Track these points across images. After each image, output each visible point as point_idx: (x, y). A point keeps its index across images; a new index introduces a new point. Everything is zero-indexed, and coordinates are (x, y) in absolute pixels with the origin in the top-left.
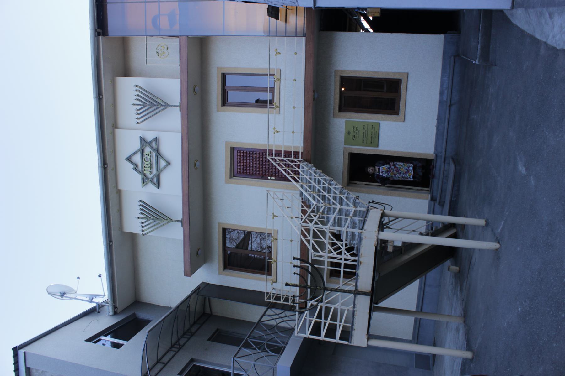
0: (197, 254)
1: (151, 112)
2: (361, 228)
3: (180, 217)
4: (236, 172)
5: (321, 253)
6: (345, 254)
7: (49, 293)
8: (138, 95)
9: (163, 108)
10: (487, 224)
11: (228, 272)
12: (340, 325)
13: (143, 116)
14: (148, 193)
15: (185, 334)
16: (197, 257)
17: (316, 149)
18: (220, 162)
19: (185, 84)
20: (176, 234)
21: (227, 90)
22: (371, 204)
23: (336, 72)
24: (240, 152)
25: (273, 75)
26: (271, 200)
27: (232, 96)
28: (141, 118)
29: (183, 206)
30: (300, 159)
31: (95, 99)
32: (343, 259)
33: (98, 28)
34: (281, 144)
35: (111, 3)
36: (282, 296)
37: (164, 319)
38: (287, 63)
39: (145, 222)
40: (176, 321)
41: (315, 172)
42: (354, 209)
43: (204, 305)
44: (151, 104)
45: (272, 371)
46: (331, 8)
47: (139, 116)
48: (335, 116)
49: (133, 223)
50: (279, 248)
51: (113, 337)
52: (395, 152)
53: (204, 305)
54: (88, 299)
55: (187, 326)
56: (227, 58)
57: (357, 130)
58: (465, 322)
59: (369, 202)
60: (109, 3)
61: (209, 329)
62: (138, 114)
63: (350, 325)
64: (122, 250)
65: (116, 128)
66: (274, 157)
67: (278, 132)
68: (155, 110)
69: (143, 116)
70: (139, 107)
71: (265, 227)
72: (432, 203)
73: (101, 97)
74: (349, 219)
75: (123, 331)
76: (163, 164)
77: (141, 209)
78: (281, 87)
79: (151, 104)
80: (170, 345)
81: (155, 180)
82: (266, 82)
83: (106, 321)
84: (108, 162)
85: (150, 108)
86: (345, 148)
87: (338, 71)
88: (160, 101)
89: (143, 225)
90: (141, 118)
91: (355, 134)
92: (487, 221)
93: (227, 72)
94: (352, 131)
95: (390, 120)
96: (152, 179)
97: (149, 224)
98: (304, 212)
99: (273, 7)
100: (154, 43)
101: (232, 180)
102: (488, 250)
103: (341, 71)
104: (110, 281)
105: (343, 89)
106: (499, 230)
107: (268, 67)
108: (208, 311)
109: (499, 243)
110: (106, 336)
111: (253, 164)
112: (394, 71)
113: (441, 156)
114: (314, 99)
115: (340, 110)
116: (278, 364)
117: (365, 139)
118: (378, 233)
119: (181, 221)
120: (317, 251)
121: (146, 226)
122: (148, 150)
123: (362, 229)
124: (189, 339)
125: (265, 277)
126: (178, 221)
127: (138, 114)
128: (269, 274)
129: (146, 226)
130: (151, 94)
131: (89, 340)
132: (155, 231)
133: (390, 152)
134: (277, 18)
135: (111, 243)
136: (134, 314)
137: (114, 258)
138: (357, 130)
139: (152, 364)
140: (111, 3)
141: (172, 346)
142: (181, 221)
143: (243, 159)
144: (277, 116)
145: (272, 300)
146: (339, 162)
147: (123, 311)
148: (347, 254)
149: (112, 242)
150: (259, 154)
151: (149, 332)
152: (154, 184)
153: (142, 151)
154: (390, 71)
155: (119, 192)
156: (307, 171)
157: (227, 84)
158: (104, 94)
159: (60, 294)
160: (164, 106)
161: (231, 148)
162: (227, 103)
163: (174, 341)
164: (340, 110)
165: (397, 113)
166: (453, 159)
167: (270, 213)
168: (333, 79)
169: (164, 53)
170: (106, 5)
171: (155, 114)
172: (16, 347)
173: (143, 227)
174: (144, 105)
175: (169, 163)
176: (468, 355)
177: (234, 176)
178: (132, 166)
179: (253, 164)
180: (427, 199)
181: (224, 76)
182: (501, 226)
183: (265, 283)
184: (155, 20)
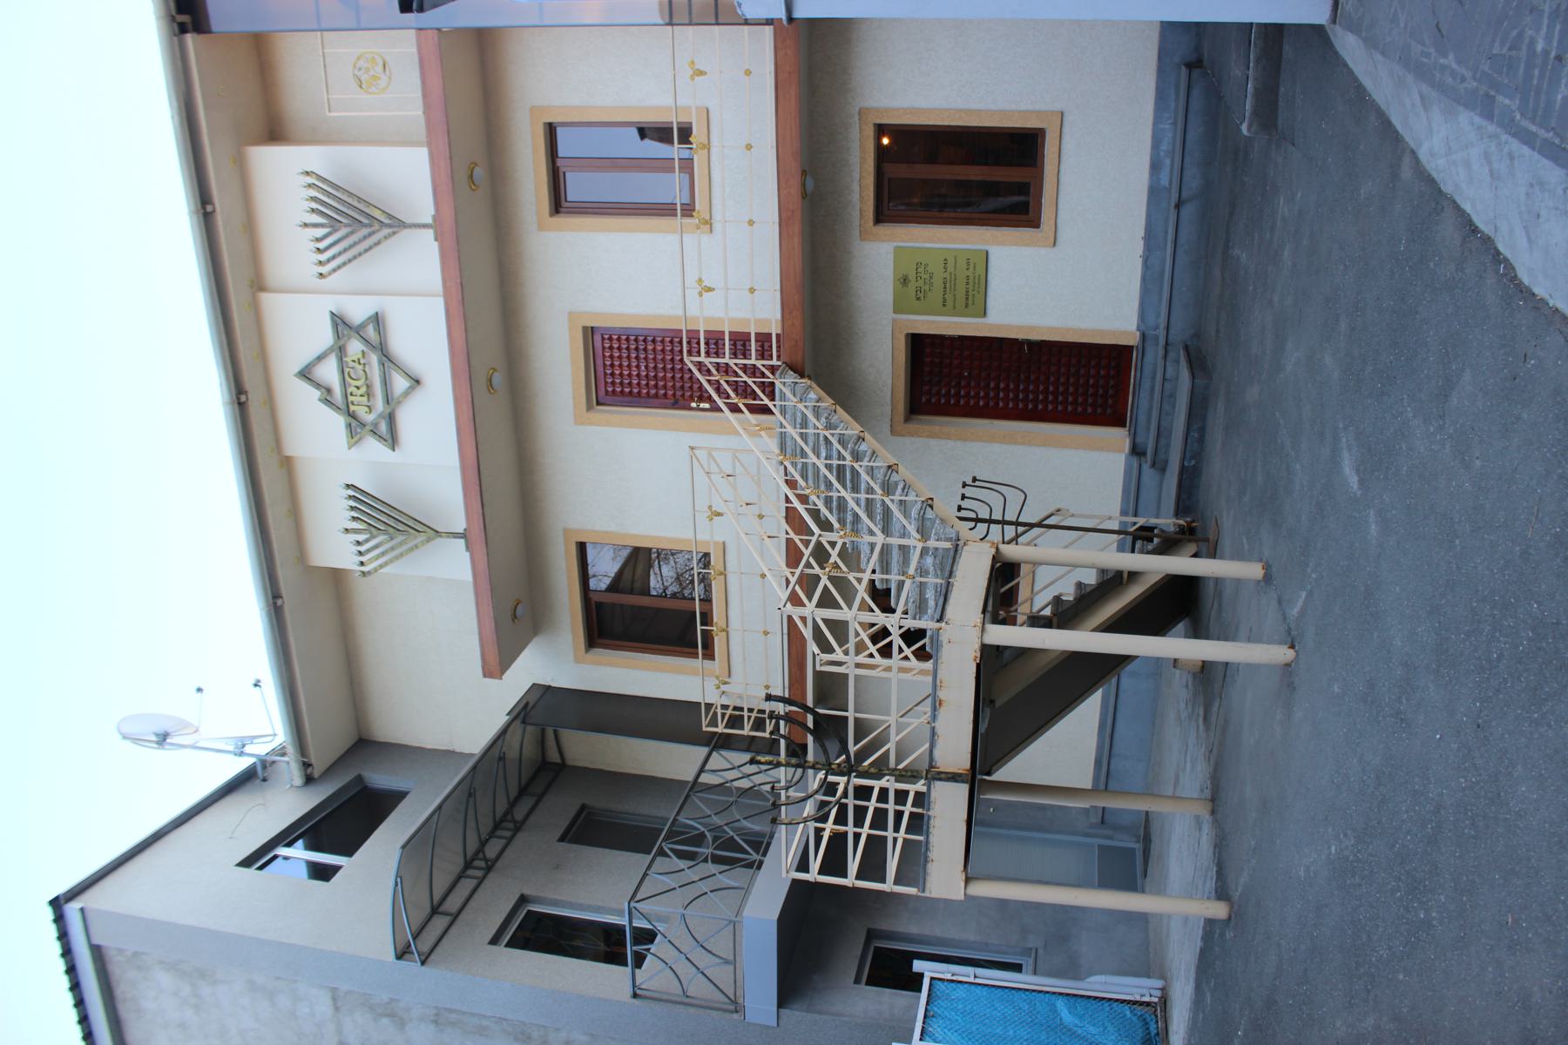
0: (515, 617)
1: (355, 244)
2: (937, 616)
3: (460, 525)
4: (602, 393)
5: (838, 655)
6: (901, 650)
7: (125, 737)
8: (314, 199)
9: (386, 231)
10: (1268, 578)
11: (600, 654)
12: (895, 840)
13: (334, 257)
14: (368, 463)
15: (497, 826)
16: (513, 618)
17: (815, 339)
18: (559, 370)
20: (452, 566)
22: (969, 492)
24: (610, 339)
26: (700, 475)
27: (578, 186)
28: (329, 261)
30: (775, 362)
31: (195, 218)
33: (180, 10)
34: (720, 314)
36: (746, 714)
37: (440, 807)
42: (920, 545)
43: (542, 742)
44: (353, 219)
47: (323, 257)
48: (864, 236)
49: (334, 542)
50: (733, 589)
51: (312, 847)
52: (1032, 328)
53: (542, 742)
54: (231, 748)
55: (502, 807)
57: (926, 271)
58: (1213, 812)
59: (965, 485)
61: (560, 808)
64: (310, 615)
66: (702, 358)
67: (710, 290)
68: (365, 238)
69: (334, 257)
70: (320, 232)
71: (689, 535)
72: (1135, 461)
73: (209, 208)
74: (908, 583)
75: (339, 824)
76: (400, 384)
77: (352, 508)
79: (353, 219)
80: (460, 861)
81: (383, 427)
83: (288, 803)
86: (894, 321)
88: (377, 214)
89: (362, 549)
90: (329, 261)
91: (921, 283)
92: (1267, 568)
94: (912, 276)
95: (1017, 244)
96: (376, 425)
97: (376, 547)
98: (793, 556)
100: (346, 50)
102: (1266, 665)
103: (877, 110)
105: (885, 141)
106: (1295, 612)
107: (671, 102)
108: (553, 756)
109: (1292, 647)
110: (289, 845)
111: (643, 370)
112: (1022, 107)
113: (1156, 338)
114: (804, 195)
115: (879, 218)
116: (746, 912)
117: (949, 297)
118: (983, 630)
119: (463, 536)
120: (830, 650)
121: (369, 551)
122: (355, 347)
123: (940, 620)
124: (509, 841)
125: (698, 663)
126: (456, 535)
129: (369, 551)
130: (351, 194)
131: (247, 863)
132: (397, 563)
133: (1020, 328)
135: (279, 602)
136: (359, 778)
137: (292, 639)
138: (926, 271)
141: (468, 865)
142: (463, 536)
143: (620, 357)
144: (705, 238)
145: (720, 729)
146: (881, 361)
147: (330, 771)
148: (908, 652)
150: (662, 341)
151: (403, 847)
154: (1013, 107)
155: (287, 463)
156: (796, 396)
157: (563, 150)
159: (154, 738)
160: (389, 226)
161: (585, 329)
162: (564, 204)
163: (471, 851)
164: (879, 218)
165: (1035, 223)
166: (1186, 348)
167: (702, 505)
168: (855, 133)
169: (375, 78)
172: (57, 898)
174: (334, 225)
175: (418, 382)
176: (1219, 910)
178: (317, 393)
179: (643, 370)
180: (1120, 451)
181: (551, 130)
182: (1300, 603)
183: (699, 680)
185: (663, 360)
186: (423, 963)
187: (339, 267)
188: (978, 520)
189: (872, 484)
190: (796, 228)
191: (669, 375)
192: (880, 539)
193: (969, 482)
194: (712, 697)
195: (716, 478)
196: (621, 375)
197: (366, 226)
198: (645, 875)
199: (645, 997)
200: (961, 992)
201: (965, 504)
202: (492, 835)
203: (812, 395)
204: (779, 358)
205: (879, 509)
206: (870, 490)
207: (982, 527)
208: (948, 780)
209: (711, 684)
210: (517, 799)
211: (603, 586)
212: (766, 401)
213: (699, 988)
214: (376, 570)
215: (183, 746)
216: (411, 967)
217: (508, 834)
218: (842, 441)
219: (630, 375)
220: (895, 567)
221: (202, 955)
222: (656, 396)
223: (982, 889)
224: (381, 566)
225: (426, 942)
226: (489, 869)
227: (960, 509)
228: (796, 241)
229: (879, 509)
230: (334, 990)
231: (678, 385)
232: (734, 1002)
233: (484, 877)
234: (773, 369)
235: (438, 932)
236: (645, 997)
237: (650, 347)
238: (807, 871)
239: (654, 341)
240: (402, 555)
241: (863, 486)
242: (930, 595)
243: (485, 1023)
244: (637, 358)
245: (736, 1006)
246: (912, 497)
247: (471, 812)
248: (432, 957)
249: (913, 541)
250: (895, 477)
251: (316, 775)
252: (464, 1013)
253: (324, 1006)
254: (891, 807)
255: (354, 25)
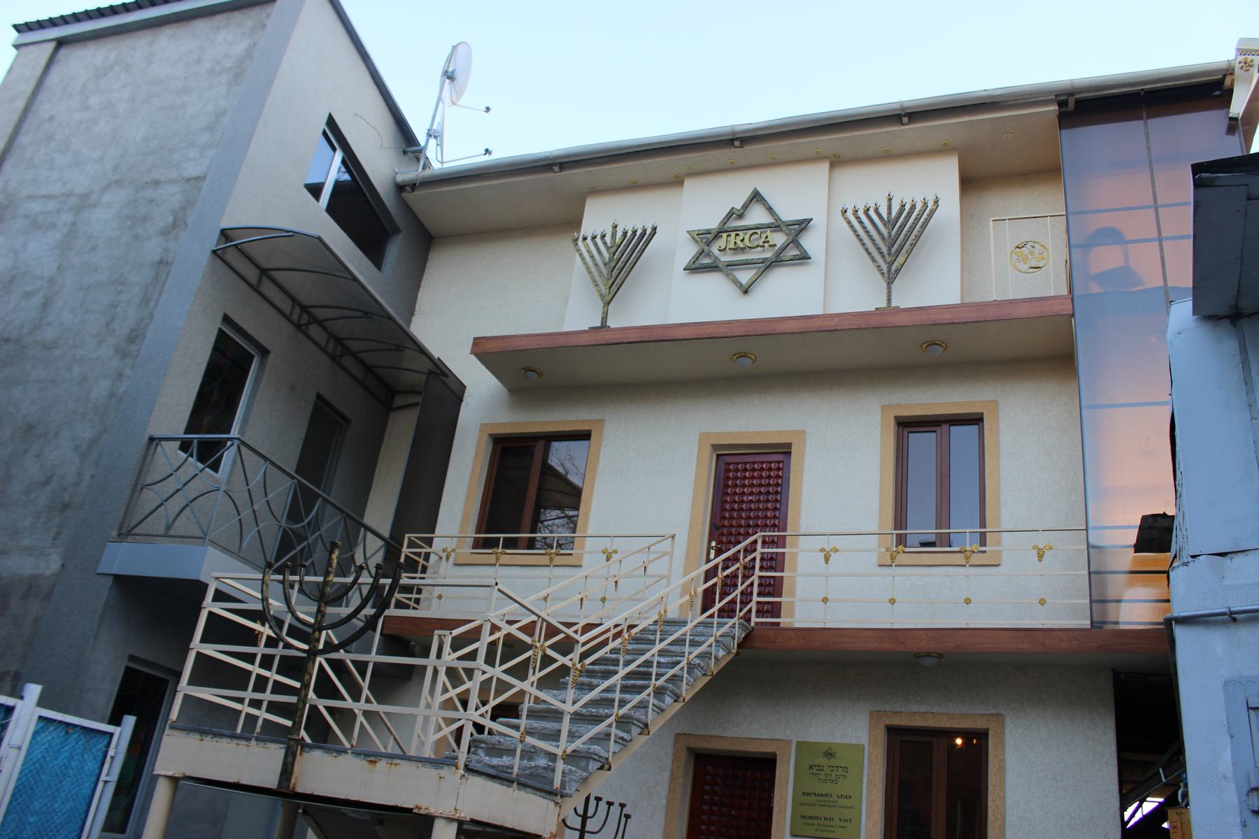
0: (527, 370)
1: (873, 241)
2: (473, 765)
3: (612, 323)
4: (729, 459)
7: (454, 47)
8: (913, 207)
9: (884, 267)
12: (241, 700)
13: (861, 222)
14: (674, 244)
15: (339, 341)
16: (527, 366)
17: (776, 663)
18: (752, 420)
19: (947, 317)
21: (938, 429)
22: (615, 810)
23: (1000, 718)
24: (779, 469)
25: (983, 542)
27: (922, 443)
28: (858, 218)
29: (640, 328)
30: (754, 620)
31: (897, 106)
32: (427, 712)
33: (1078, 102)
34: (801, 568)
35: (1147, 134)
37: (355, 279)
38: (1016, 584)
39: (605, 243)
40: (361, 314)
41: (705, 656)
42: (559, 752)
44: (894, 240)
45: (201, 535)
46: (1177, 685)
47: (861, 214)
50: (537, 571)
51: (338, 185)
54: (435, 127)
55: (355, 346)
56: (1023, 432)
57: (838, 776)
60: (1146, 126)
61: (348, 399)
62: (867, 211)
63: (239, 730)
64: (540, 197)
65: (833, 165)
67: (827, 560)
68: (878, 249)
69: (861, 222)
73: (905, 120)
74: (516, 734)
76: (745, 276)
77: (635, 232)
78: (951, 570)
79: (894, 240)
80: (306, 302)
81: (706, 261)
82: (963, 529)
83: (382, 167)
84: (747, 148)
85: (883, 238)
87: (1003, 724)
88: (900, 259)
89: (598, 240)
90: (858, 218)
93: (986, 427)
94: (833, 762)
96: (709, 255)
97: (599, 251)
99: (1169, 530)
101: (707, 451)
103: (1002, 733)
104: (470, 170)
108: (399, 401)
110: (344, 162)
111: (749, 495)
114: (918, 656)
115: (892, 731)
117: (812, 799)
118: (450, 820)
119: (604, 326)
121: (596, 245)
122: (779, 239)
123: (468, 769)
124: (324, 350)
125: (471, 533)
126: (604, 319)
127: (867, 211)
128: (478, 544)
129: (596, 245)
130: (918, 237)
131: (331, 122)
134: (1139, 547)
135: (556, 169)
136: (397, 231)
138: (838, 776)
139: (258, 253)
140: (1147, 134)
141: (304, 309)
142: (604, 326)
143: (761, 477)
144: (873, 558)
147: (406, 207)
149: (561, 169)
150: (775, 517)
151: (320, 239)
152: (696, 258)
153: (777, 226)
155: (677, 182)
157: (955, 430)
158: (911, 126)
160: (889, 271)
161: (789, 445)
163: (316, 312)
164: (892, 731)
167: (618, 544)
169: (1025, 260)
170: (1140, 118)
171: (867, 250)
173: (594, 238)
174: (890, 223)
175: (746, 292)
177: (718, 456)
179: (749, 495)
181: (976, 420)
184: (1110, 236)
185: (758, 517)
186: (214, 252)
187: (852, 227)
188: (585, 818)
189: (629, 706)
190: (887, 645)
191: (743, 522)
192: (569, 708)
193: (626, 811)
194: (438, 544)
195: (643, 557)
196: (745, 478)
197: (889, 250)
198: (266, 459)
199: (148, 449)
200: (91, 765)
201: (603, 805)
202: (331, 335)
203: (721, 653)
204: (757, 623)
205: (602, 711)
206: (623, 703)
207: (577, 823)
208: (285, 764)
209: (450, 544)
210: (361, 362)
211: (554, 461)
212: (718, 606)
213: (149, 499)
214: (578, 250)
215: (441, 91)
216: (212, 241)
217: (330, 349)
218: (675, 679)
219: (744, 486)
220: (537, 724)
221: (252, 80)
222: (724, 509)
223: (162, 794)
224: (581, 255)
225: (232, 256)
226: (298, 327)
227: (598, 799)
228: (873, 645)
229: (602, 711)
230: (204, 177)
231: (733, 530)
232: (129, 533)
233: (291, 322)
234: (747, 618)
235: (242, 271)
236: (148, 449)
237: (770, 505)
238: (215, 599)
239: (775, 509)
240: (590, 273)
241: (627, 696)
242: (505, 760)
243: (152, 304)
244: (760, 493)
245: (125, 534)
246: (613, 747)
247: (353, 313)
248: (219, 261)
249: (563, 746)
250: (635, 731)
251: (404, 195)
252: (163, 285)
253: (192, 170)
254: (267, 696)
255: (1073, 242)
